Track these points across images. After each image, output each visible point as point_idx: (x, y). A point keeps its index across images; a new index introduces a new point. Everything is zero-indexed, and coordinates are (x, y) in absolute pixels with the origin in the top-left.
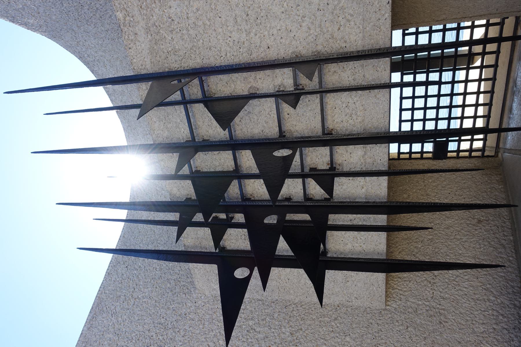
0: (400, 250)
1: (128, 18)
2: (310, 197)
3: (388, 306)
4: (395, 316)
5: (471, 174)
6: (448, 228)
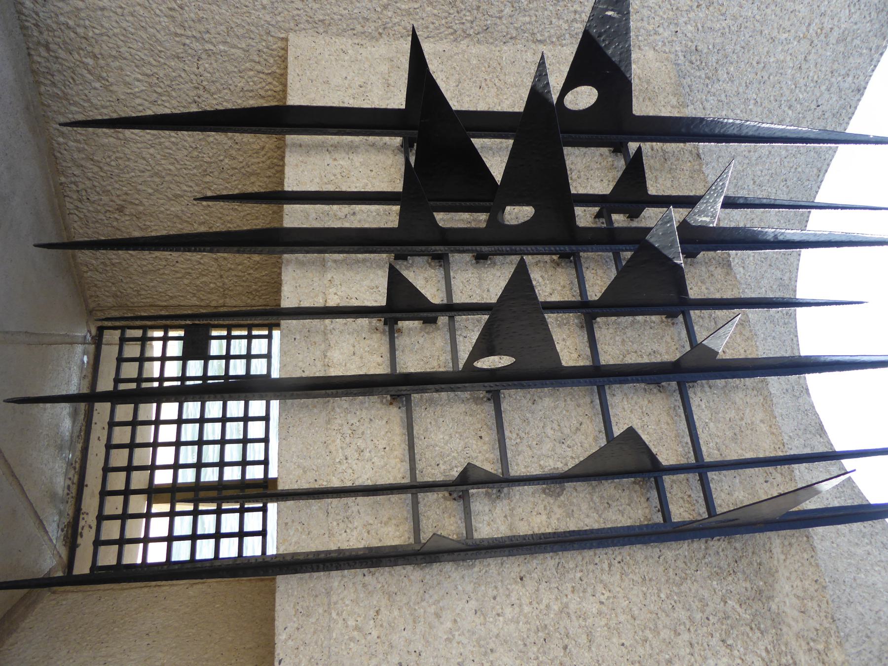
0: (263, 153)
1: (821, 647)
2: (436, 261)
3: (282, 39)
4: (268, 18)
5: (142, 297)
6: (177, 196)
